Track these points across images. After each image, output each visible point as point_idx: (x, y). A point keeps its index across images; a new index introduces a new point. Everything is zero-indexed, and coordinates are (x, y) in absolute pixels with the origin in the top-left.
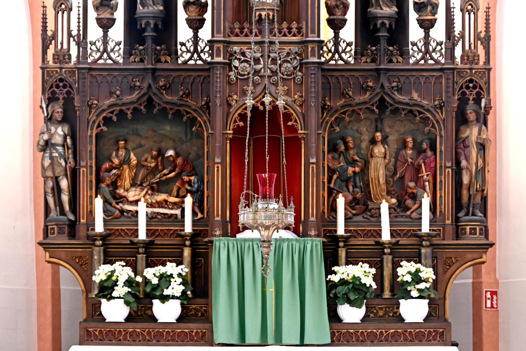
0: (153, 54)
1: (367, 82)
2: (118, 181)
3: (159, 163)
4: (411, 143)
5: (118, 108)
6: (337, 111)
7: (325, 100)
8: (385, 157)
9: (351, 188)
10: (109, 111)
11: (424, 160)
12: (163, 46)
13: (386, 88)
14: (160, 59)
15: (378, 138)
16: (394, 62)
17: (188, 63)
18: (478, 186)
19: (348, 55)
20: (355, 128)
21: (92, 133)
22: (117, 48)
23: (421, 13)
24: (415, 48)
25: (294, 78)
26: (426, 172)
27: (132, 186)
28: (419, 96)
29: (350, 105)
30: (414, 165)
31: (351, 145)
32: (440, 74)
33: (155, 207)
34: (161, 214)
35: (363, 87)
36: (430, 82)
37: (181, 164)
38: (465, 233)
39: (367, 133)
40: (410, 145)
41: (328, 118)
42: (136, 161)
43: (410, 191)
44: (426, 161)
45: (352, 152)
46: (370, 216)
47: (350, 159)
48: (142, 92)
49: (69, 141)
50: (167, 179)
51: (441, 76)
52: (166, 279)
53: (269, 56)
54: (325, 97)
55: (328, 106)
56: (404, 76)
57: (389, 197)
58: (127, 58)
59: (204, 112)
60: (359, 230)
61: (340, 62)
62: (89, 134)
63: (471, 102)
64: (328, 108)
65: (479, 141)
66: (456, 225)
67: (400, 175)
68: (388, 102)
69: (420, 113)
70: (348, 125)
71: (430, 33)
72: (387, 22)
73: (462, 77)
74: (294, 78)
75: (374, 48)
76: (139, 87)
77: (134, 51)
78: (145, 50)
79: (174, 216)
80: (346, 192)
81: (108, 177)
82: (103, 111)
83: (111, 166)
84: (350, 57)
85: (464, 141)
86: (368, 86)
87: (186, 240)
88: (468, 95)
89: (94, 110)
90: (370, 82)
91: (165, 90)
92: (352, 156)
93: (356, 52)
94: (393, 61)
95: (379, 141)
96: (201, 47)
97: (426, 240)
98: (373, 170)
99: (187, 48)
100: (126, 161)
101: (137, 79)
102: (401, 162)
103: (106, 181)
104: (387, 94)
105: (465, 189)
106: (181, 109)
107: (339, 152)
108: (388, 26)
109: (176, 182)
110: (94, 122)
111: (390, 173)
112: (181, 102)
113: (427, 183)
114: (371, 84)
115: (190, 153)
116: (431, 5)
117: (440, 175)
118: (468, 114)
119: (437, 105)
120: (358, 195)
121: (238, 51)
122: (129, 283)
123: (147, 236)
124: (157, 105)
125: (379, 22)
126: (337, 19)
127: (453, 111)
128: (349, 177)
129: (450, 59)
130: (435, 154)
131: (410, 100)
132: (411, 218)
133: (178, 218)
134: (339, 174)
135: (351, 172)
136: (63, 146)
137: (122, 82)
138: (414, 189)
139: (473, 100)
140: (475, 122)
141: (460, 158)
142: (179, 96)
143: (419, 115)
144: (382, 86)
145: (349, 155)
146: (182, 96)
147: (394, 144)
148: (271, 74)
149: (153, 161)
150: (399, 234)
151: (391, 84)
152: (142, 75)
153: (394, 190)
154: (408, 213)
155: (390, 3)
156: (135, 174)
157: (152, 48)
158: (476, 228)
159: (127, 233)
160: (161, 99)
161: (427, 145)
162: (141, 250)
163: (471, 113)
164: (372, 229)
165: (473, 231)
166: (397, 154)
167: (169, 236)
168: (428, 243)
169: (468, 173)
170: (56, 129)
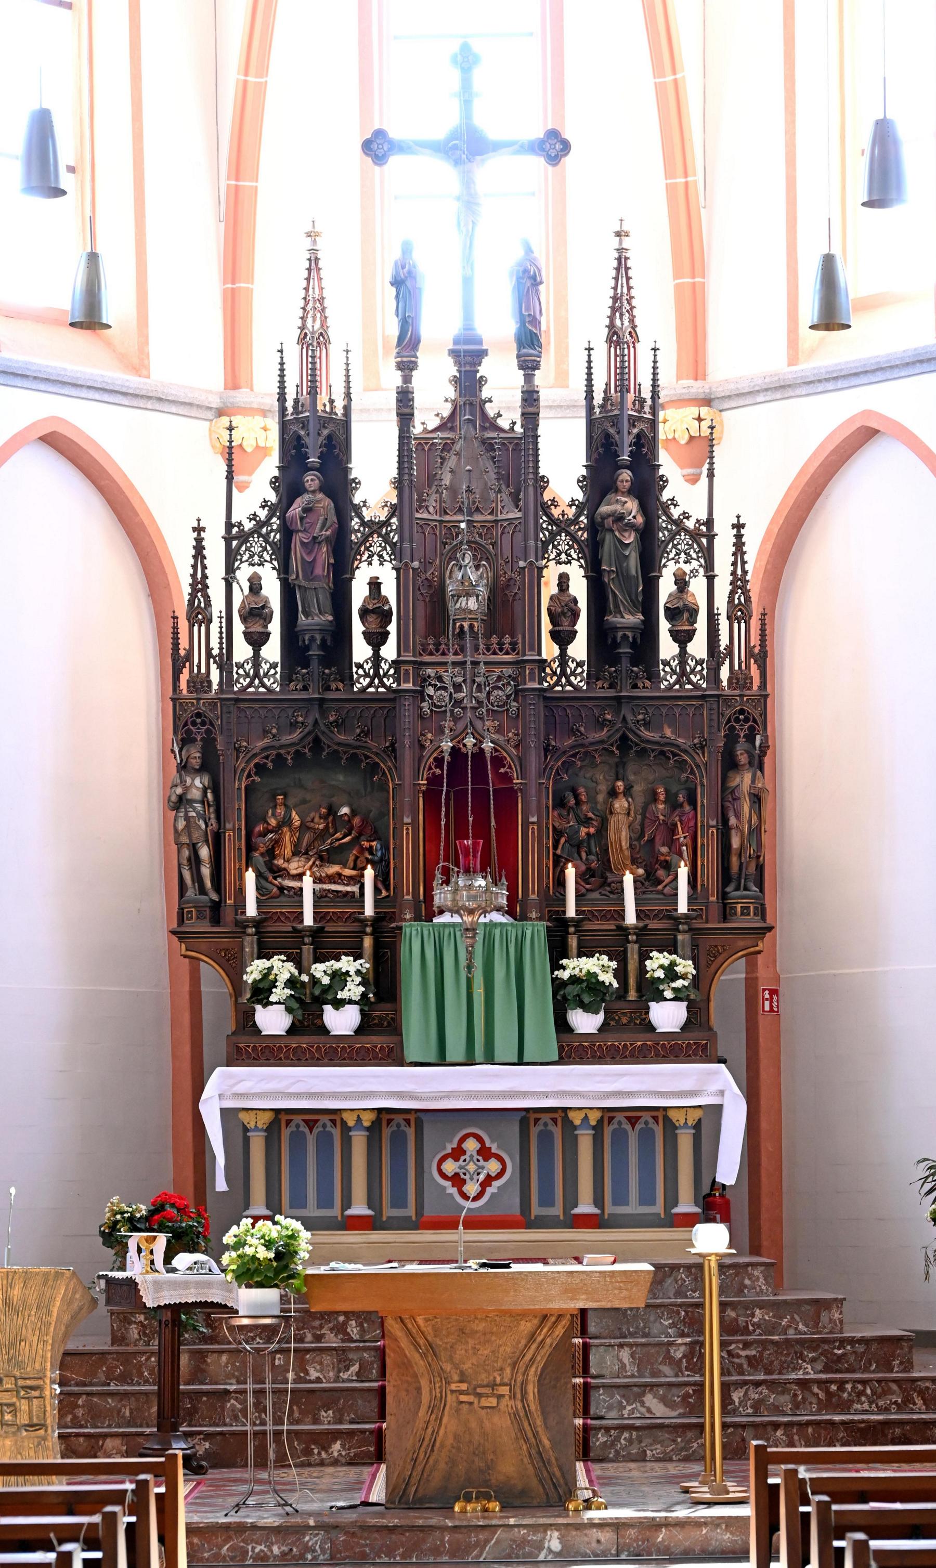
5: (275, 752)
6: (564, 753)
8: (628, 814)
9: (584, 855)
10: (263, 755)
19: (579, 679)
20: (588, 775)
21: (240, 785)
22: (272, 671)
23: (674, 623)
24: (667, 669)
25: (507, 710)
29: (582, 745)
33: (325, 883)
38: (735, 914)
40: (662, 797)
43: (662, 858)
47: (582, 817)
48: (306, 730)
49: (210, 795)
50: (340, 845)
52: (340, 978)
53: (474, 681)
55: (553, 746)
59: (388, 756)
62: (236, 786)
63: (742, 740)
65: (752, 791)
69: (675, 755)
71: (688, 649)
72: (630, 634)
73: (729, 706)
74: (507, 710)
76: (302, 723)
82: (255, 755)
83: (267, 828)
84: (581, 681)
85: (733, 792)
86: (605, 720)
97: (683, 924)
100: (286, 822)
106: (358, 752)
108: (631, 639)
110: (243, 770)
112: (358, 743)
113: (684, 848)
114: (609, 717)
115: (371, 811)
116: (688, 610)
121: (433, 675)
122: (291, 983)
123: (315, 920)
124: (326, 747)
125: (620, 634)
135: (583, 834)
136: (202, 802)
140: (747, 766)
146: (359, 735)
148: (477, 705)
154: (660, 887)
162: (307, 940)
163: (741, 754)
166: (645, 809)
168: (686, 927)
169: (739, 834)
170: (193, 780)
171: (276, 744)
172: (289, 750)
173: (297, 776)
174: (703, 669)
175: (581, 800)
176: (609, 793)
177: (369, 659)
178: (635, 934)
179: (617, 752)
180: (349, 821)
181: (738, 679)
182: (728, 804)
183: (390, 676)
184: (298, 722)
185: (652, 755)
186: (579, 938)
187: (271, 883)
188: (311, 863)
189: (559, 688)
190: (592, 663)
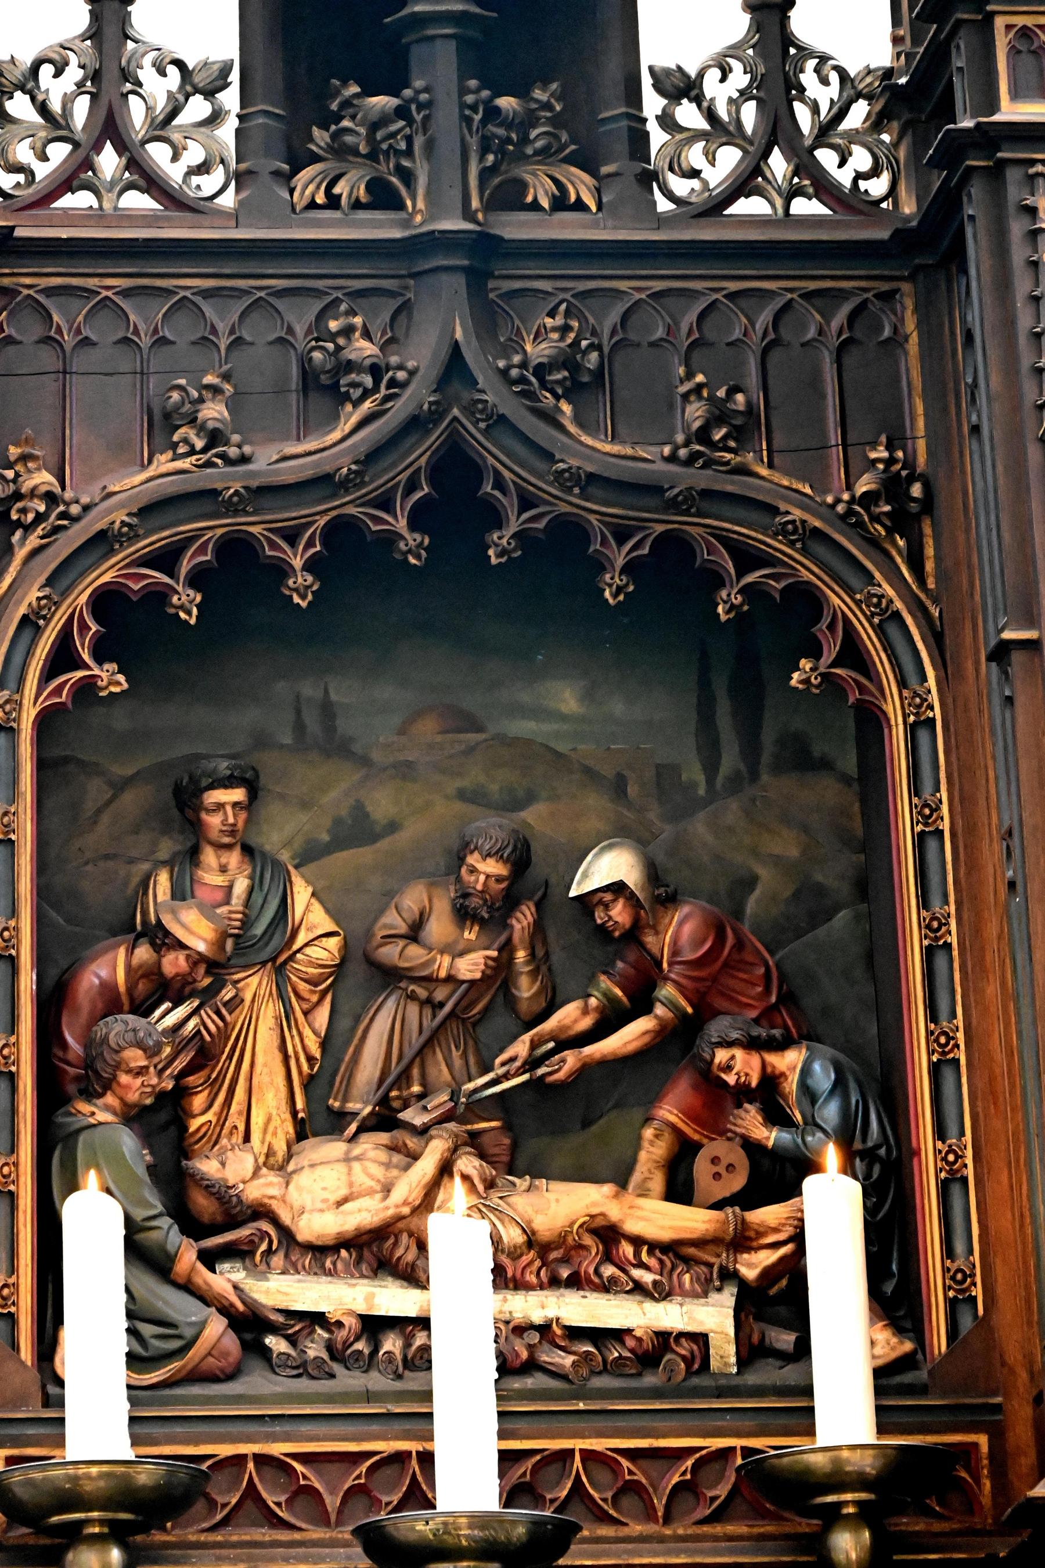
0: (474, 143)
2: (198, 1102)
3: (521, 955)
5: (216, 528)
10: (144, 545)
12: (538, 94)
14: (522, 186)
17: (729, 211)
22: (197, 108)
24: (688, 115)
27: (302, 1132)
34: (576, 1333)
37: (689, 956)
42: (333, 943)
48: (400, 409)
50: (586, 1069)
58: (277, 174)
59: (873, 543)
61: (137, 201)
76: (376, 371)
77: (321, 137)
78: (410, 122)
79: (684, 1348)
81: (140, 1045)
83: (153, 972)
84: (203, 168)
87: (832, 1516)
89: (33, 541)
91: (573, 391)
96: (815, 109)
99: (711, 115)
101: (358, 320)
103: (124, 1078)
109: (654, 1098)
112: (701, 478)
114: (363, 349)
115: (750, 882)
124: (509, 504)
133: (714, 1364)
137: (238, 342)
142: (680, 438)
146: (703, 435)
149: (470, 935)
152: (391, 294)
156: (325, 1044)
157: (463, 105)
159: (310, 1491)
160: (549, 457)
167: (659, 1504)
171: (219, 477)
172: (291, 514)
173: (309, 690)
177: (734, 51)
180: (633, 935)
183: (853, 136)
184: (350, 366)
187: (188, 1287)
188: (427, 1166)
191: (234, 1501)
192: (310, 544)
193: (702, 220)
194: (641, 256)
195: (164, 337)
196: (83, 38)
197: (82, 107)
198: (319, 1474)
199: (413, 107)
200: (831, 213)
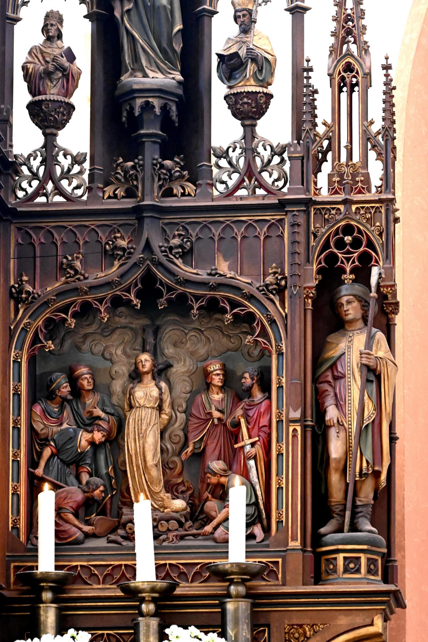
1: (115, 238)
4: (218, 375)
6: (46, 304)
7: (21, 281)
8: (160, 408)
9: (85, 478)
11: (246, 411)
13: (157, 250)
15: (143, 366)
16: (176, 196)
18: (365, 464)
20: (98, 349)
23: (232, 83)
24: (223, 163)
26: (250, 437)
28: (230, 268)
30: (225, 425)
31: (85, 383)
32: (278, 217)
35: (106, 251)
36: (256, 236)
38: (335, 571)
39: (124, 358)
40: (217, 380)
41: (25, 321)
43: (214, 480)
44: (251, 413)
45: (90, 400)
46: (122, 537)
47: (85, 416)
51: (281, 221)
54: (22, 276)
55: (28, 292)
56: (199, 223)
57: (169, 495)
60: (94, 566)
61: (58, 199)
63: (348, 277)
64: (27, 299)
65: (365, 361)
66: (314, 552)
67: (194, 448)
68: (162, 284)
69: (234, 304)
70: (84, 343)
71: (258, 129)
72: (156, 103)
73: (327, 221)
75: (130, 164)
80: (73, 485)
85: (334, 366)
86: (116, 248)
88: (342, 262)
90: (122, 238)
92: (89, 409)
93: (91, 176)
94: (175, 191)
95: (147, 373)
97: (237, 584)
98: (132, 436)
102: (198, 418)
104: (159, 264)
105: (336, 470)
107: (58, 399)
108: (157, 111)
111: (174, 446)
113: (252, 463)
114: (123, 243)
116: (254, 60)
117: (278, 441)
118: (343, 305)
119: (271, 284)
120: (97, 492)
125: (139, 102)
126: (46, 100)
127: (308, 297)
128: (81, 453)
129: (301, 183)
130: (269, 398)
131: (210, 274)
132: (215, 540)
134: (56, 447)
135: (84, 443)
138: (221, 476)
139: (351, 272)
140: (360, 324)
141: (324, 403)
143: (232, 309)
144: (148, 246)
145: (84, 409)
147: (185, 380)
150: (184, 573)
151: (167, 241)
153: (183, 483)
154: (208, 528)
155: (165, 64)
158: (359, 558)
161: (252, 379)
163: (348, 302)
164: (123, 563)
165: (352, 565)
166: (190, 402)
168: (241, 589)
169: (342, 435)
174: (283, 161)
175: (82, 388)
176: (130, 376)
178: (154, 600)
179: (136, 302)
181: (341, 175)
182: (326, 386)
185: (196, 306)
186: (59, 610)
189: (42, 199)
190: (97, 159)
191: (118, 577)
192: (106, 303)
193: (226, 198)
194: (258, 209)
195: (199, 237)
196: (42, 147)
197: (242, 161)
198: (185, 567)
199: (137, 166)
200: (66, 201)
